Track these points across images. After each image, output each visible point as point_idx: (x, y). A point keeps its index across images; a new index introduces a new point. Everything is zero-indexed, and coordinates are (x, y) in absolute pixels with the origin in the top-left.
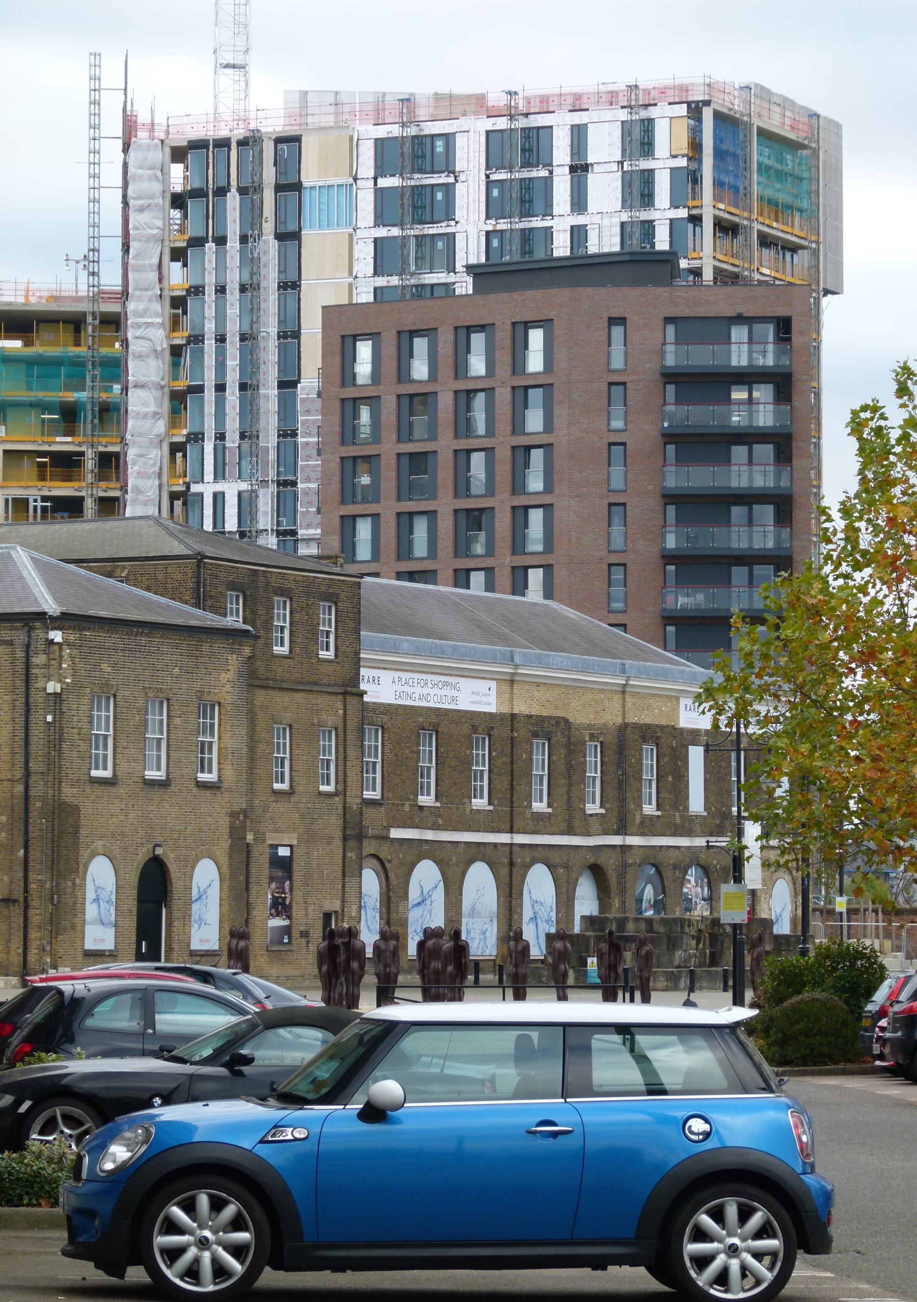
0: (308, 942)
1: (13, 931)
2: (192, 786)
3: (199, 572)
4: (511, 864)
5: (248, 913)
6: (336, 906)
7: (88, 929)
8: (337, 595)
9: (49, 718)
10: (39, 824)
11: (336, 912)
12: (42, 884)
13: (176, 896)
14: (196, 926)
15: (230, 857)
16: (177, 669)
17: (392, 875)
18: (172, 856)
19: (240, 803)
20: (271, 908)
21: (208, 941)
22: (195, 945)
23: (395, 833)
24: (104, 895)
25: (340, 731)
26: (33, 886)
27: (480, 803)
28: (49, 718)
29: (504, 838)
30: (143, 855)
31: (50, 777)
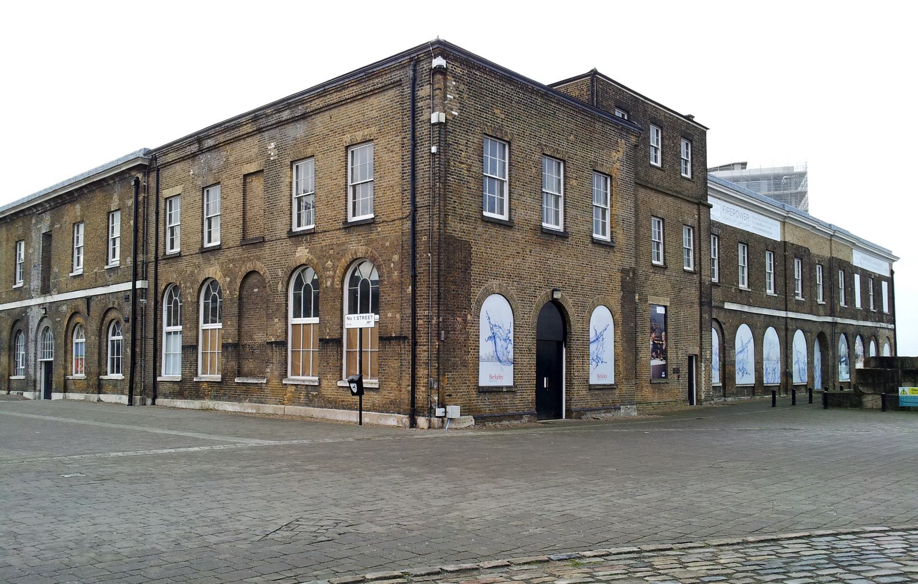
0: (679, 377)
1: (404, 368)
2: (588, 241)
3: (593, 86)
4: (787, 329)
5: (637, 355)
6: (697, 351)
7: (482, 366)
8: (693, 136)
9: (434, 149)
10: (425, 257)
11: (696, 355)
12: (429, 319)
13: (575, 337)
14: (594, 363)
15: (622, 306)
16: (572, 137)
17: (726, 332)
18: (570, 301)
19: (629, 263)
20: (652, 352)
21: (605, 377)
22: (593, 381)
23: (728, 306)
24: (501, 333)
25: (696, 229)
26: (420, 322)
27: (770, 292)
28: (434, 149)
29: (782, 314)
30: (542, 297)
31: (436, 210)
